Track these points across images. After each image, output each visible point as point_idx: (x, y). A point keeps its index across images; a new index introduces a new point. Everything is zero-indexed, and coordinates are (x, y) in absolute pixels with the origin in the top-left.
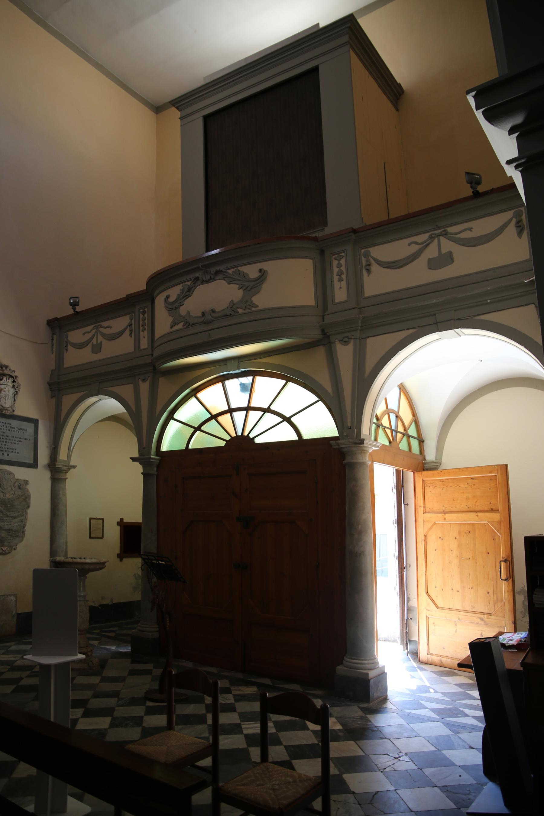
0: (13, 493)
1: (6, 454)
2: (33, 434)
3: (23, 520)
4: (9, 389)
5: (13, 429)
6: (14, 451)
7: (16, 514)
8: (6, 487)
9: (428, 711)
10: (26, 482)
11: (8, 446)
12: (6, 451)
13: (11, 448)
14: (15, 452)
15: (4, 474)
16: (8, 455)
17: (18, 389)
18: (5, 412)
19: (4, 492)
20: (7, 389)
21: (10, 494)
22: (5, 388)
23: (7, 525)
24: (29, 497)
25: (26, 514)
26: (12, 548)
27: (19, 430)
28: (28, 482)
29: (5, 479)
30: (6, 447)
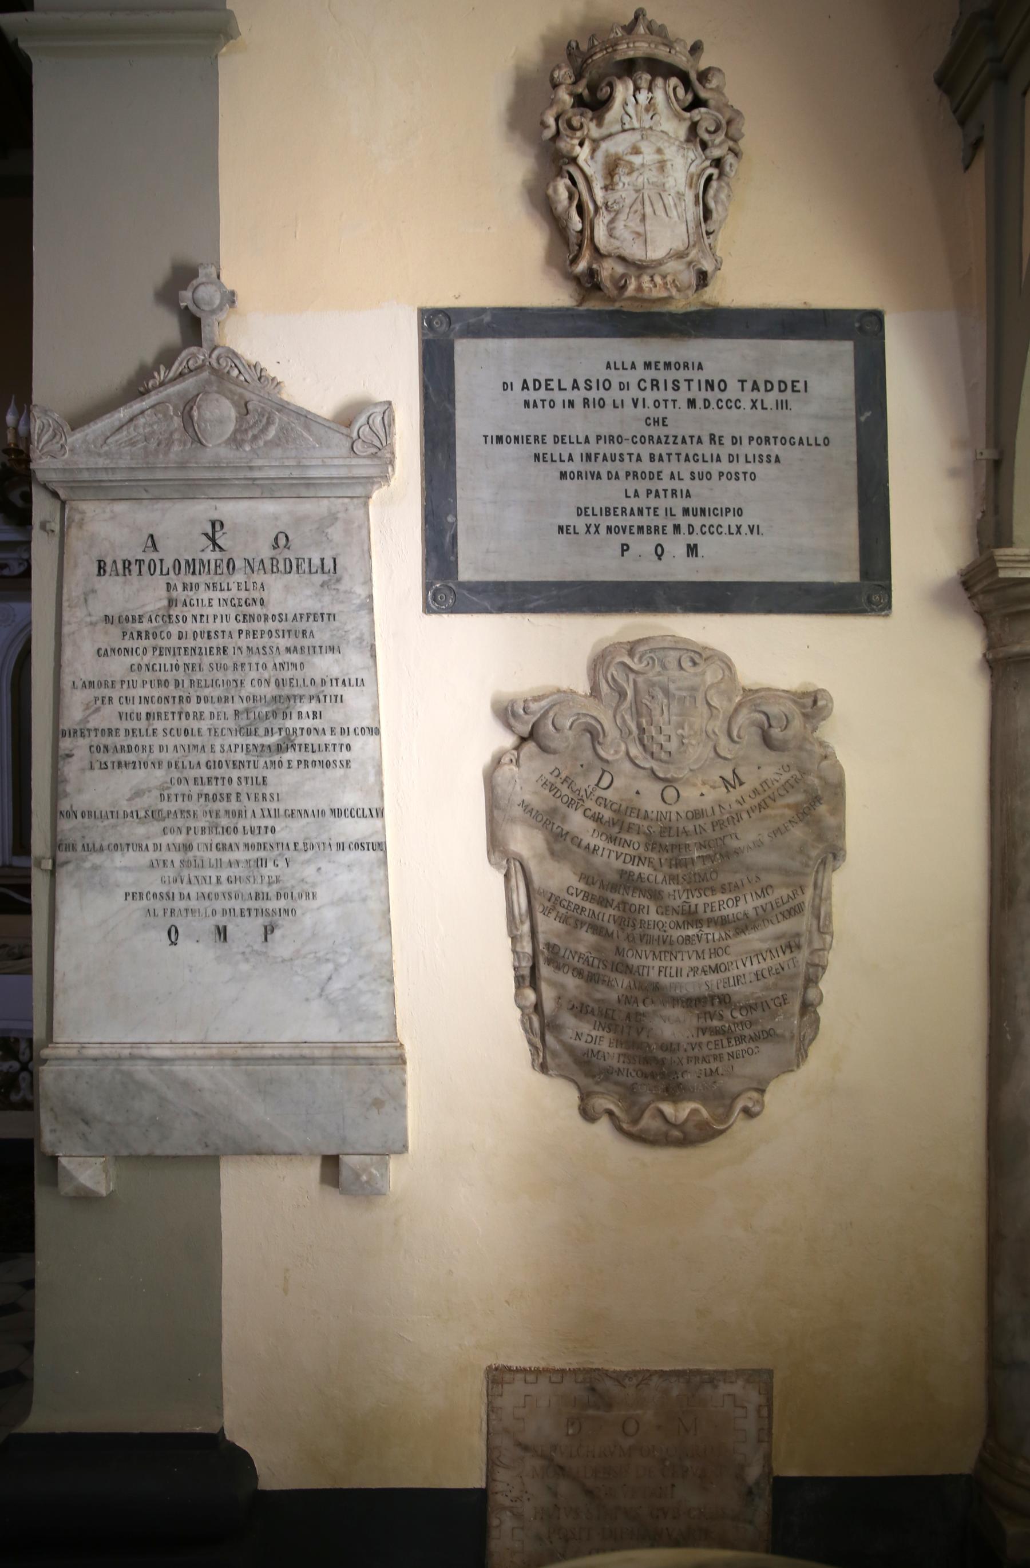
0: (729, 776)
1: (676, 546)
2: (851, 405)
3: (798, 935)
4: (659, 151)
5: (713, 396)
6: (732, 520)
7: (749, 905)
8: (673, 746)
9: (683, 240)
10: (809, 701)
11: (688, 495)
12: (677, 528)
13: (708, 505)
14: (739, 528)
15: (658, 668)
16: (692, 550)
17: (720, 137)
18: (640, 288)
19: (661, 775)
20: (648, 155)
21: (704, 783)
22: (636, 151)
23: (694, 970)
24: (836, 790)
25: (822, 897)
26: (730, 1109)
27: (755, 395)
28: (820, 703)
29: (667, 693)
30: (678, 504)
